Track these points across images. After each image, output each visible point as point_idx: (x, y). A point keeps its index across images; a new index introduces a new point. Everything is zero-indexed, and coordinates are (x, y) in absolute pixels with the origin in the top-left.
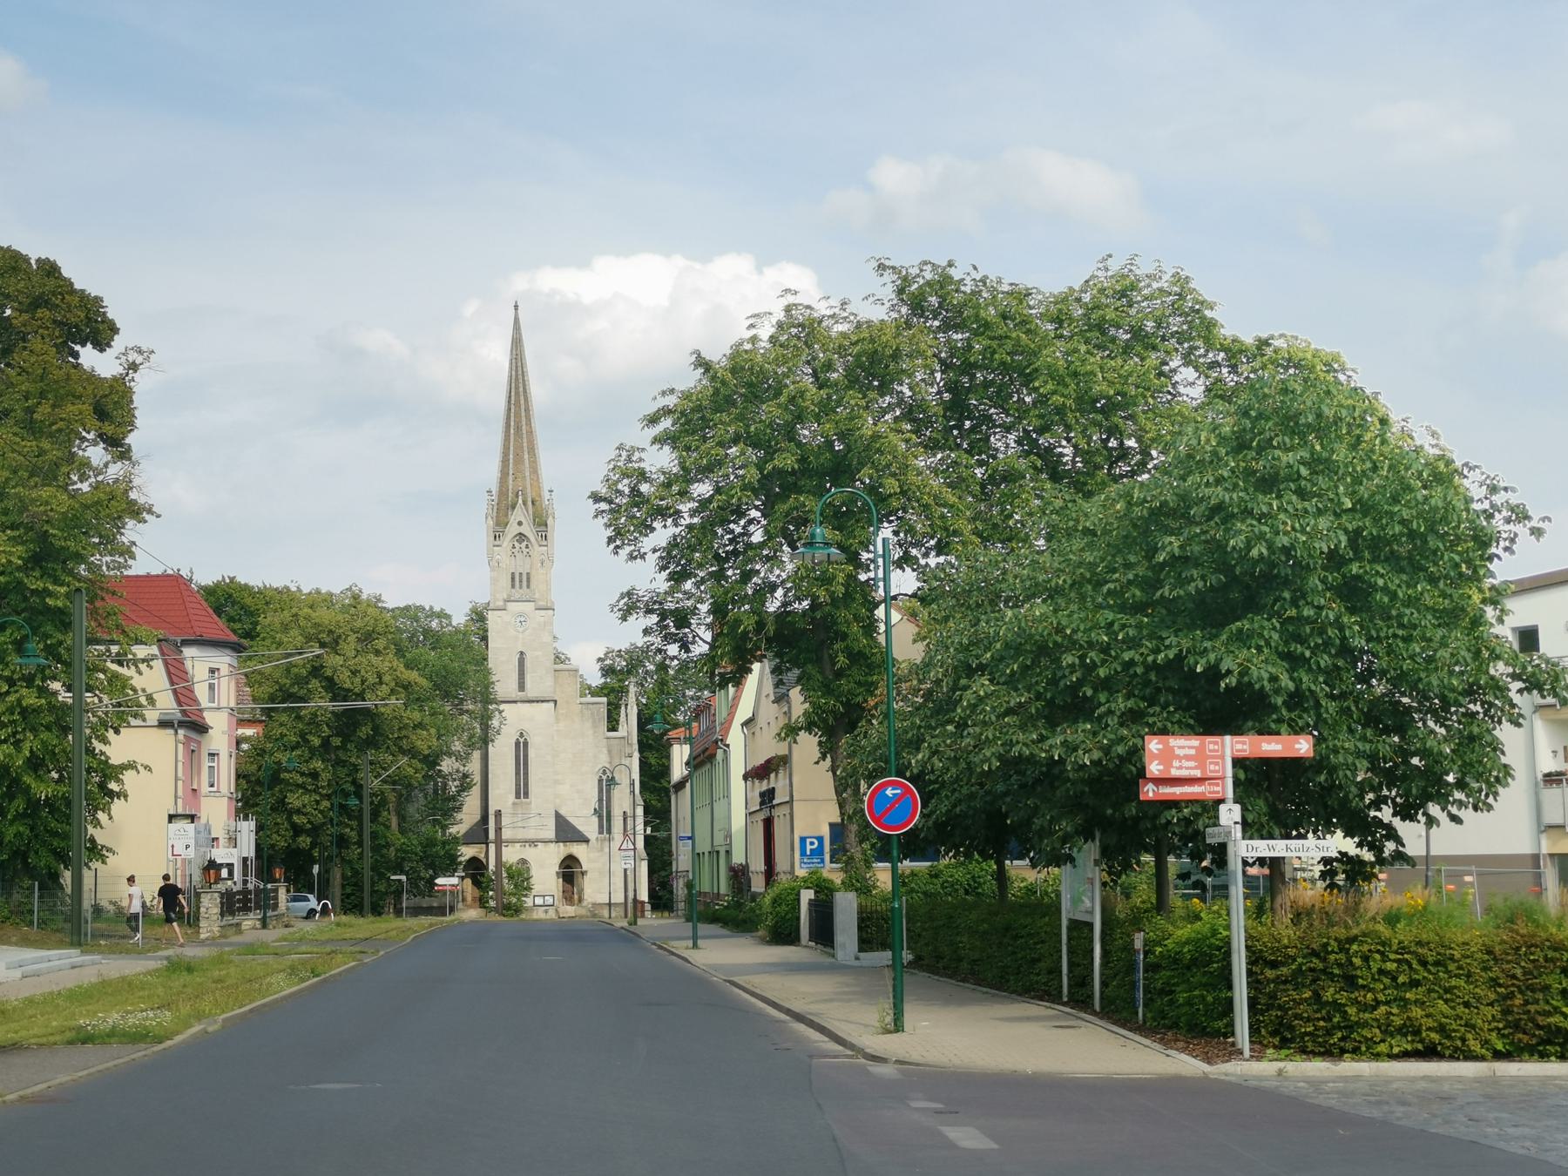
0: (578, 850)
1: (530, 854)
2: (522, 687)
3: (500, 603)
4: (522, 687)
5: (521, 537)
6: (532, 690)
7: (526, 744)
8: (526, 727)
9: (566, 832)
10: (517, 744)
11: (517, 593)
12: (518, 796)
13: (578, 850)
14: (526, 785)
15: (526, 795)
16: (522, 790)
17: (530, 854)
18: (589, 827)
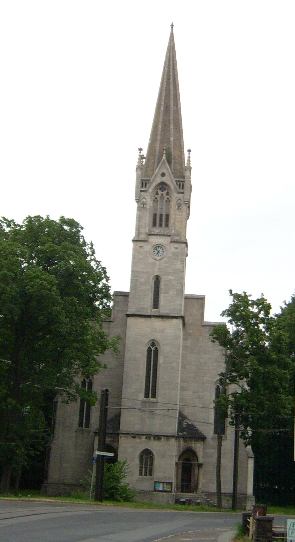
0: (198, 447)
1: (154, 446)
2: (156, 305)
4: (156, 305)
5: (163, 186)
6: (163, 310)
7: (156, 351)
8: (158, 337)
9: (188, 432)
10: (149, 350)
11: (157, 230)
12: (147, 396)
13: (198, 447)
14: (154, 386)
15: (154, 396)
16: (151, 390)
17: (154, 446)
18: (209, 431)
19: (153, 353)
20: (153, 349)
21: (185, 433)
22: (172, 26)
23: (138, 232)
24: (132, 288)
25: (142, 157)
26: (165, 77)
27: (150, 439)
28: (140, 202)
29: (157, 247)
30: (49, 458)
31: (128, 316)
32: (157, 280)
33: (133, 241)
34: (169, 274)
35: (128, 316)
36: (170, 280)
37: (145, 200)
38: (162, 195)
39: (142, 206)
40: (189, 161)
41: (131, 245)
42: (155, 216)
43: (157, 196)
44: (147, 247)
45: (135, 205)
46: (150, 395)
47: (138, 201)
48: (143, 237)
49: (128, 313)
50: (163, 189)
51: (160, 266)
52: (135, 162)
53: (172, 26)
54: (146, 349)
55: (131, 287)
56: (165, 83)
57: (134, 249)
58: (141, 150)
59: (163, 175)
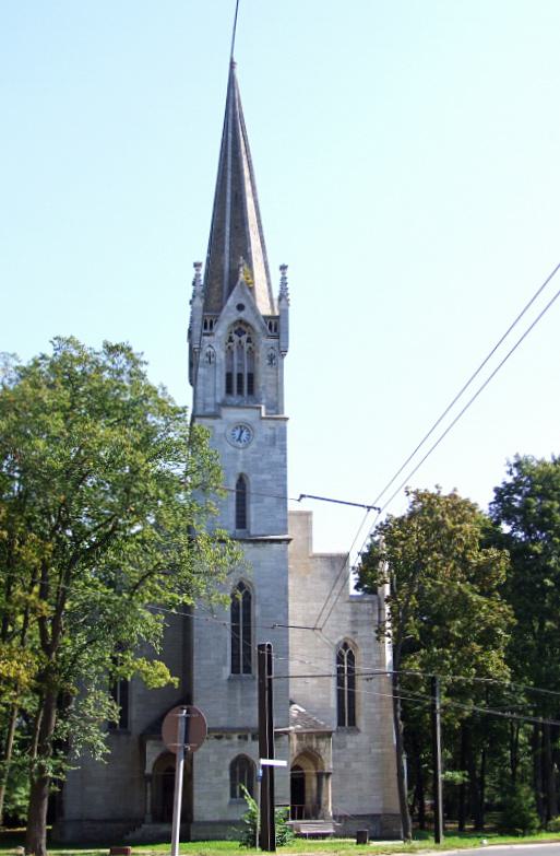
3: (211, 410)
4: (242, 521)
8: (250, 575)
12: (235, 669)
27: (246, 738)
34: (262, 471)
36: (264, 481)
38: (240, 342)
42: (229, 376)
43: (230, 344)
46: (241, 669)
50: (240, 333)
51: (245, 457)
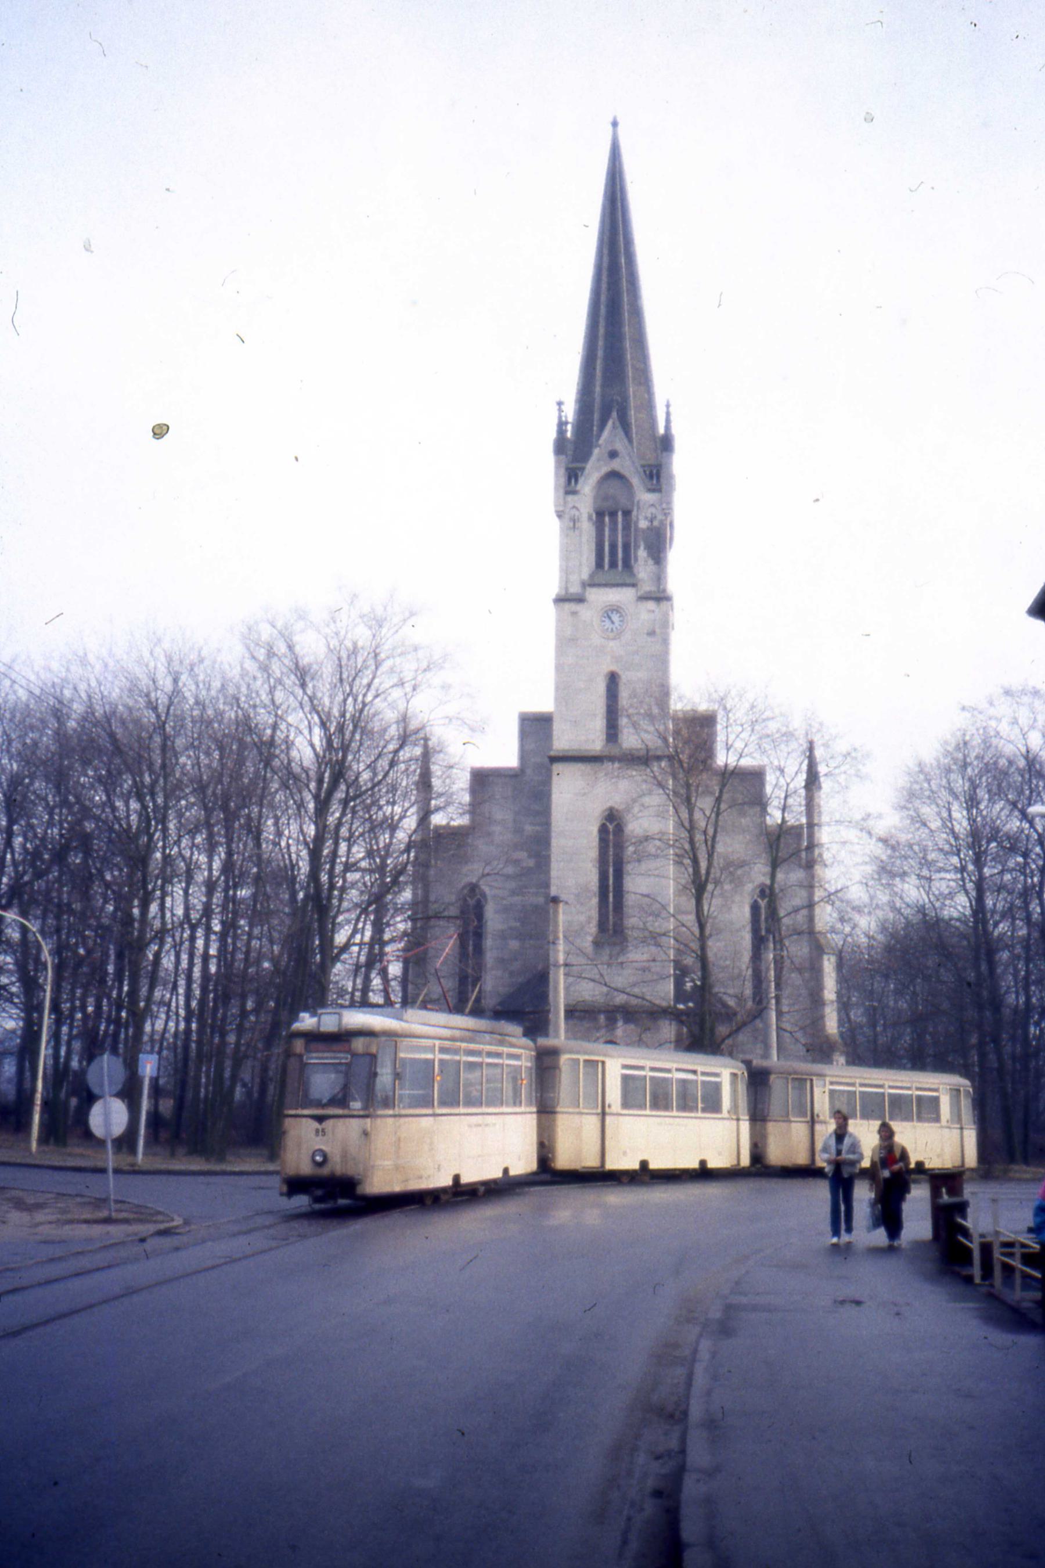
10: (603, 830)
19: (612, 828)
20: (611, 827)
21: (691, 1005)
22: (615, 124)
23: (566, 582)
24: (558, 700)
25: (561, 425)
26: (606, 259)
28: (567, 516)
29: (611, 611)
30: (437, 1011)
31: (554, 759)
32: (613, 679)
33: (559, 600)
35: (554, 759)
37: (577, 513)
39: (571, 524)
40: (668, 421)
41: (550, 611)
44: (587, 613)
45: (555, 524)
47: (560, 515)
48: (575, 589)
49: (552, 753)
52: (551, 434)
53: (615, 124)
54: (595, 830)
55: (556, 699)
56: (604, 278)
57: (559, 621)
58: (560, 404)
59: (613, 455)
